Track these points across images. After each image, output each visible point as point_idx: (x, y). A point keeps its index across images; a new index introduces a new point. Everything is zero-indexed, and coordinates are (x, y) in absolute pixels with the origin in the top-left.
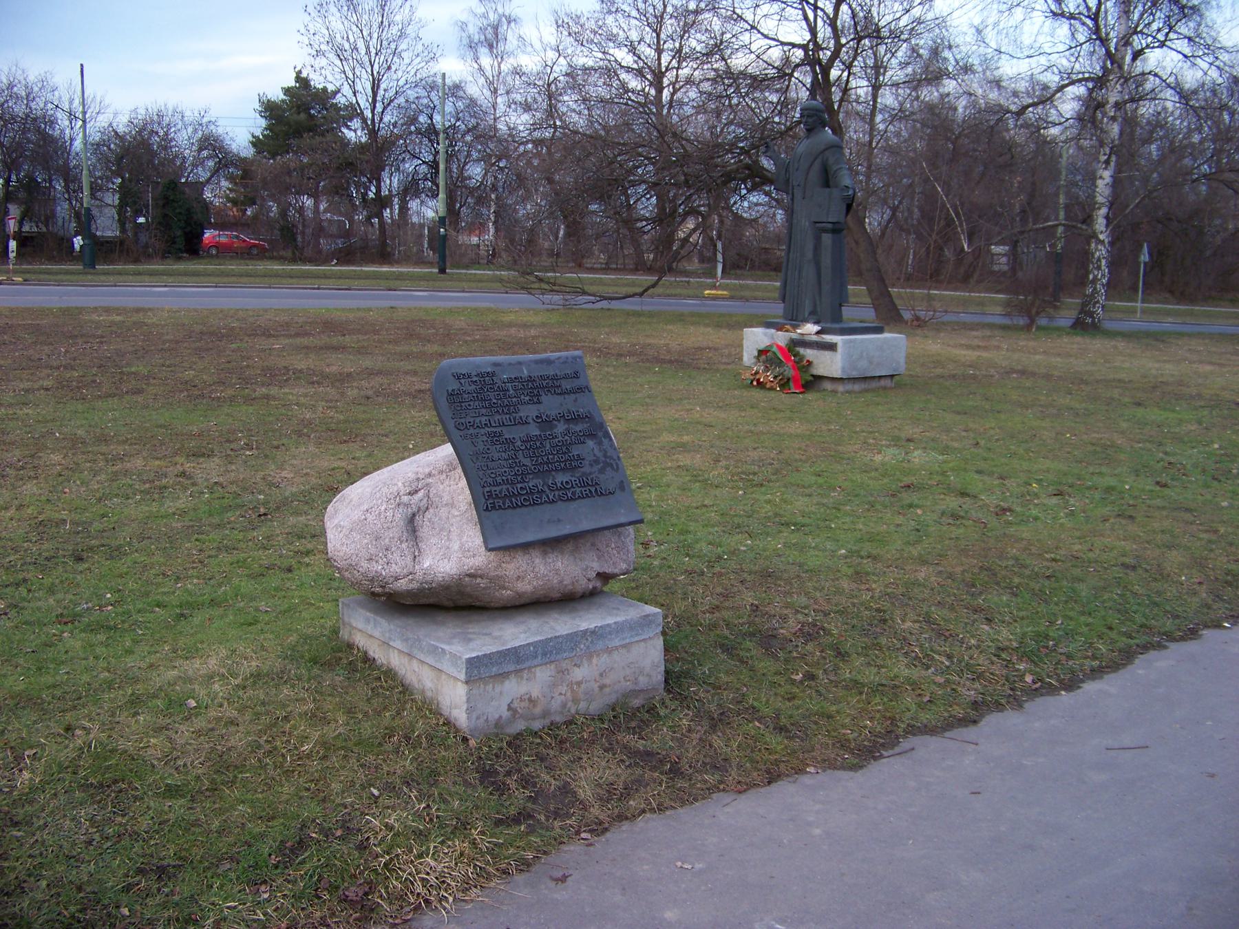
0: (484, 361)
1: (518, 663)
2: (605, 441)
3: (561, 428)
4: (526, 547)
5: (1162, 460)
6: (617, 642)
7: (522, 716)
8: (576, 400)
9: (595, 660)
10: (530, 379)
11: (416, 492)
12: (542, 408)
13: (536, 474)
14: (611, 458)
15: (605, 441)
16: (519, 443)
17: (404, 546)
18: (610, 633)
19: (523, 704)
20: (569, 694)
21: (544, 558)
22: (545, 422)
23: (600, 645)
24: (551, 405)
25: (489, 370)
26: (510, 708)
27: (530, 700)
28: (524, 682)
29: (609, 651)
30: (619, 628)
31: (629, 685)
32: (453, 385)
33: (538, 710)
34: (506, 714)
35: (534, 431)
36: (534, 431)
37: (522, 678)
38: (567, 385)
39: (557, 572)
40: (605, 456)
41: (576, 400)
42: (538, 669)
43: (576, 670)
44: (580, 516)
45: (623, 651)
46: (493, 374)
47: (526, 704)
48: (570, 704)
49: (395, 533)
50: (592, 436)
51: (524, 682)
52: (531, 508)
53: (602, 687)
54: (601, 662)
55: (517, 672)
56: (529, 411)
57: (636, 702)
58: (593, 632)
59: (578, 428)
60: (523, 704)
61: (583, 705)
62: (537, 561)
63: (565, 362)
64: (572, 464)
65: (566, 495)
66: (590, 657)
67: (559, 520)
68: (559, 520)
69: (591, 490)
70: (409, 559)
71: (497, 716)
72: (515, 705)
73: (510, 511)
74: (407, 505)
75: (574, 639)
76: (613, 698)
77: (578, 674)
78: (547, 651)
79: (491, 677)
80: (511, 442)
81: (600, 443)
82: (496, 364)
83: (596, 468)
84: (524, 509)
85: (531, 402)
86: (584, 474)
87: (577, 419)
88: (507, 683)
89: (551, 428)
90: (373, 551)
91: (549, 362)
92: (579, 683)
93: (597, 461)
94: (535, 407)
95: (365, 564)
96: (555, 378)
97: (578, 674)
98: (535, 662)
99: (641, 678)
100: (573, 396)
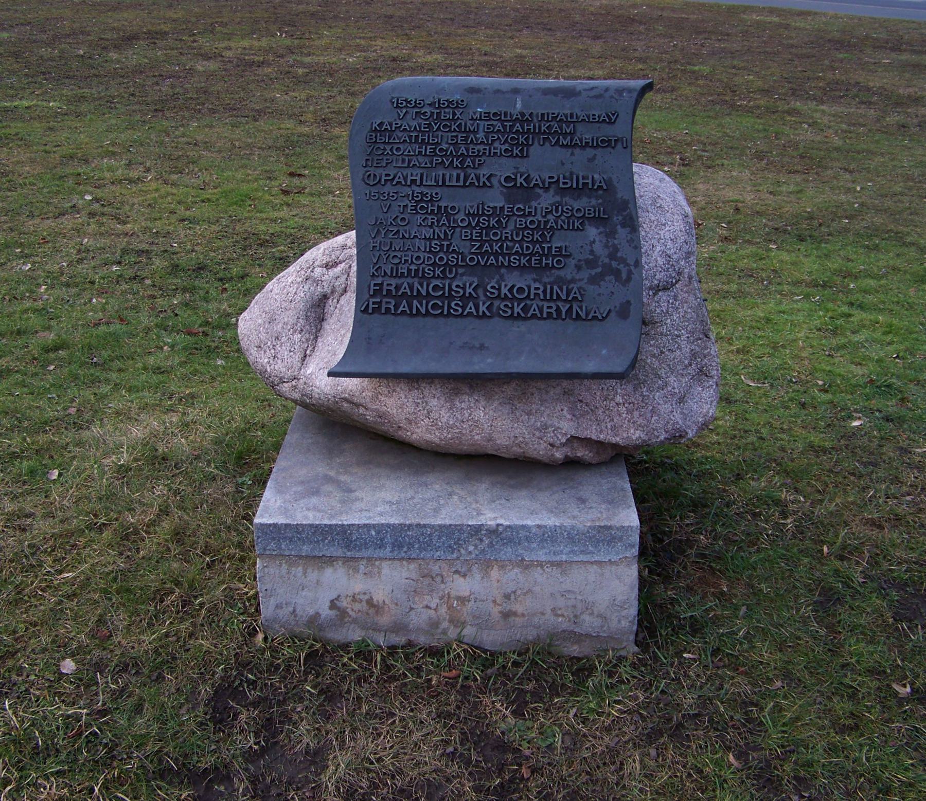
0: (451, 83)
1: (348, 547)
2: (622, 232)
3: (546, 200)
4: (414, 380)
5: (765, 225)
6: (542, 556)
7: (355, 621)
8: (591, 160)
9: (495, 573)
10: (523, 119)
11: (336, 264)
12: (523, 166)
13: (472, 269)
14: (623, 261)
15: (622, 232)
16: (461, 216)
17: (297, 337)
18: (528, 539)
19: (357, 606)
20: (443, 610)
21: (450, 400)
22: (520, 190)
23: (507, 552)
24: (544, 161)
25: (457, 97)
26: (333, 605)
27: (370, 602)
28: (360, 576)
29: (525, 565)
30: (547, 536)
31: (563, 624)
32: (388, 117)
33: (384, 620)
34: (326, 612)
35: (495, 199)
36: (495, 199)
37: (356, 570)
38: (586, 133)
39: (477, 424)
40: (612, 256)
41: (591, 160)
42: (385, 564)
43: (459, 580)
44: (527, 348)
45: (556, 571)
46: (458, 105)
47: (364, 607)
48: (445, 624)
49: (289, 317)
50: (599, 220)
51: (360, 576)
52: (441, 320)
53: (506, 615)
54: (513, 578)
55: (347, 560)
56: (502, 168)
57: (574, 650)
58: (494, 532)
59: (581, 203)
60: (357, 606)
61: (469, 632)
62: (434, 402)
63: (597, 97)
64: (540, 263)
65: (520, 310)
66: (487, 566)
67: (482, 347)
68: (482, 347)
69: (567, 309)
70: (298, 357)
71: (312, 612)
72: (344, 604)
73: (405, 319)
74: (317, 282)
75: (455, 537)
76: (531, 634)
77: (461, 586)
78: (400, 541)
79: (300, 557)
80: (446, 212)
81: (611, 234)
82: (473, 90)
83: (585, 274)
84: (429, 321)
85: (509, 154)
86: (560, 281)
87: (582, 189)
88: (329, 571)
89: (527, 201)
90: (263, 336)
91: (570, 93)
92: (463, 600)
93: (591, 263)
94: (511, 162)
95: (254, 351)
96: (572, 120)
97: (461, 586)
98: (381, 553)
99: (586, 617)
100: (590, 152)
